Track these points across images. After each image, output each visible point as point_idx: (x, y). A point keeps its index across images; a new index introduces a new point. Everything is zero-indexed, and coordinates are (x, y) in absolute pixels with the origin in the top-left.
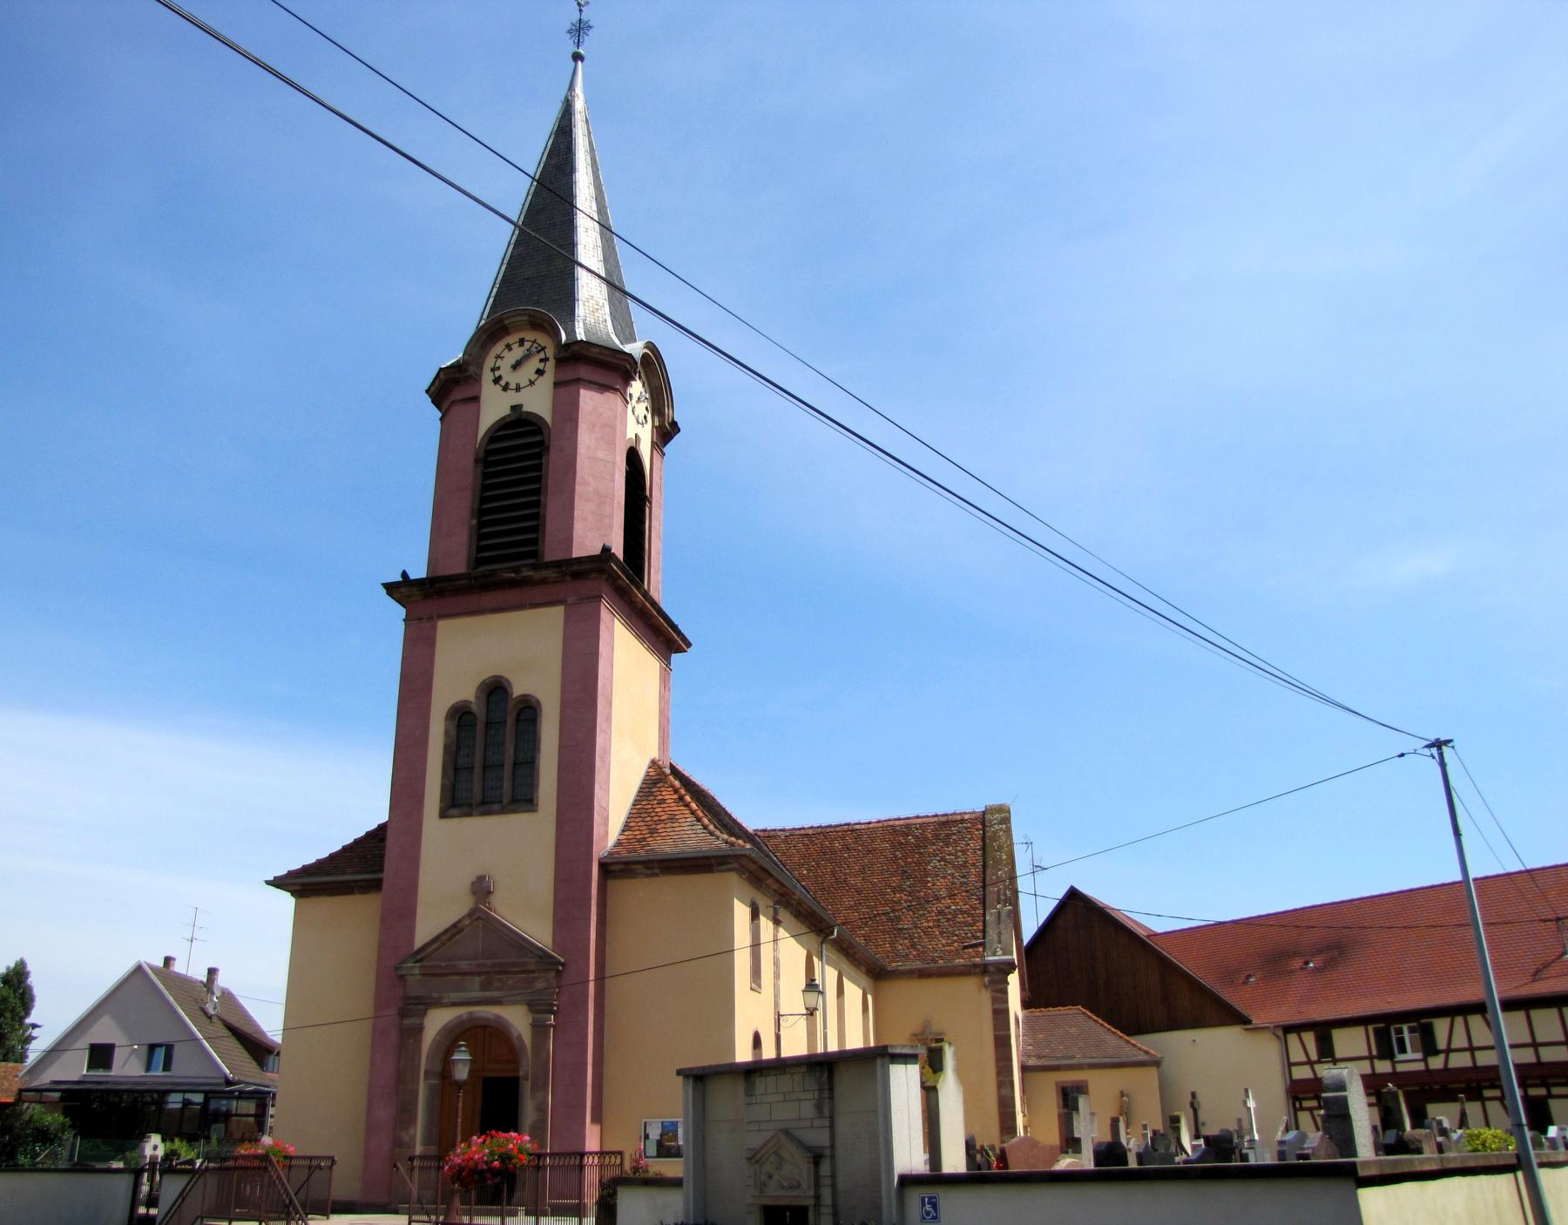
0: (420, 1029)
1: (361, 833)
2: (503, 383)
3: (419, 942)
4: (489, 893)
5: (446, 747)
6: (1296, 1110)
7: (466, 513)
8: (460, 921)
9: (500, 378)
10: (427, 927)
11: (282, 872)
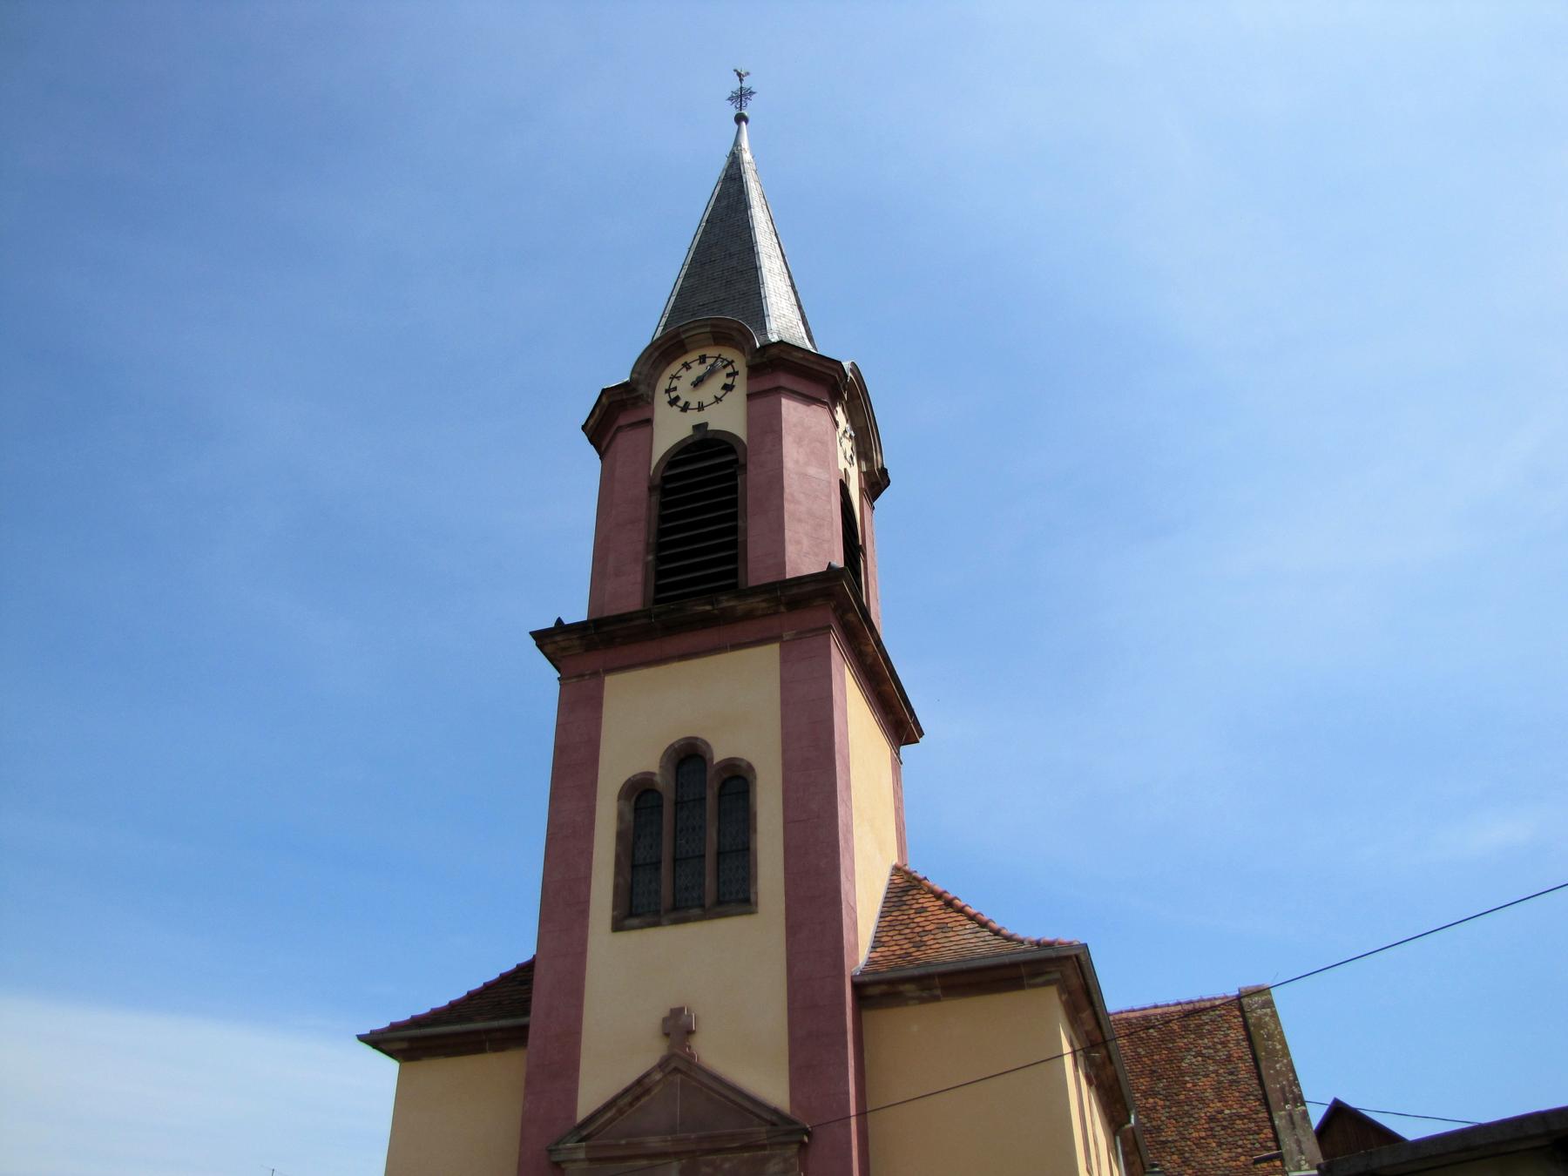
1: (493, 975)
2: (681, 403)
3: (582, 1112)
5: (620, 836)
7: (641, 547)
9: (677, 398)
10: (595, 1089)
11: (382, 1023)
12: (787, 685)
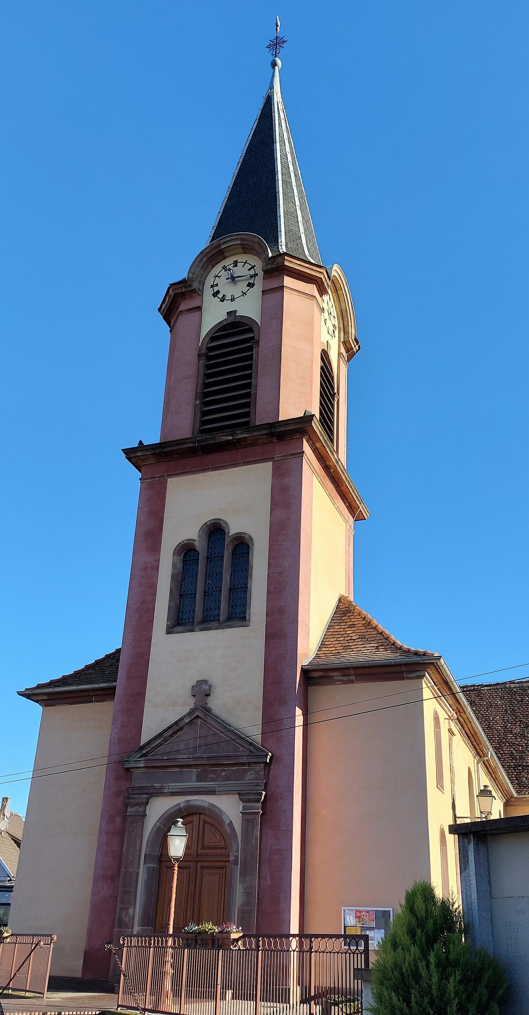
2: (220, 296)
5: (173, 577)
8: (181, 719)
9: (218, 292)
10: (153, 722)
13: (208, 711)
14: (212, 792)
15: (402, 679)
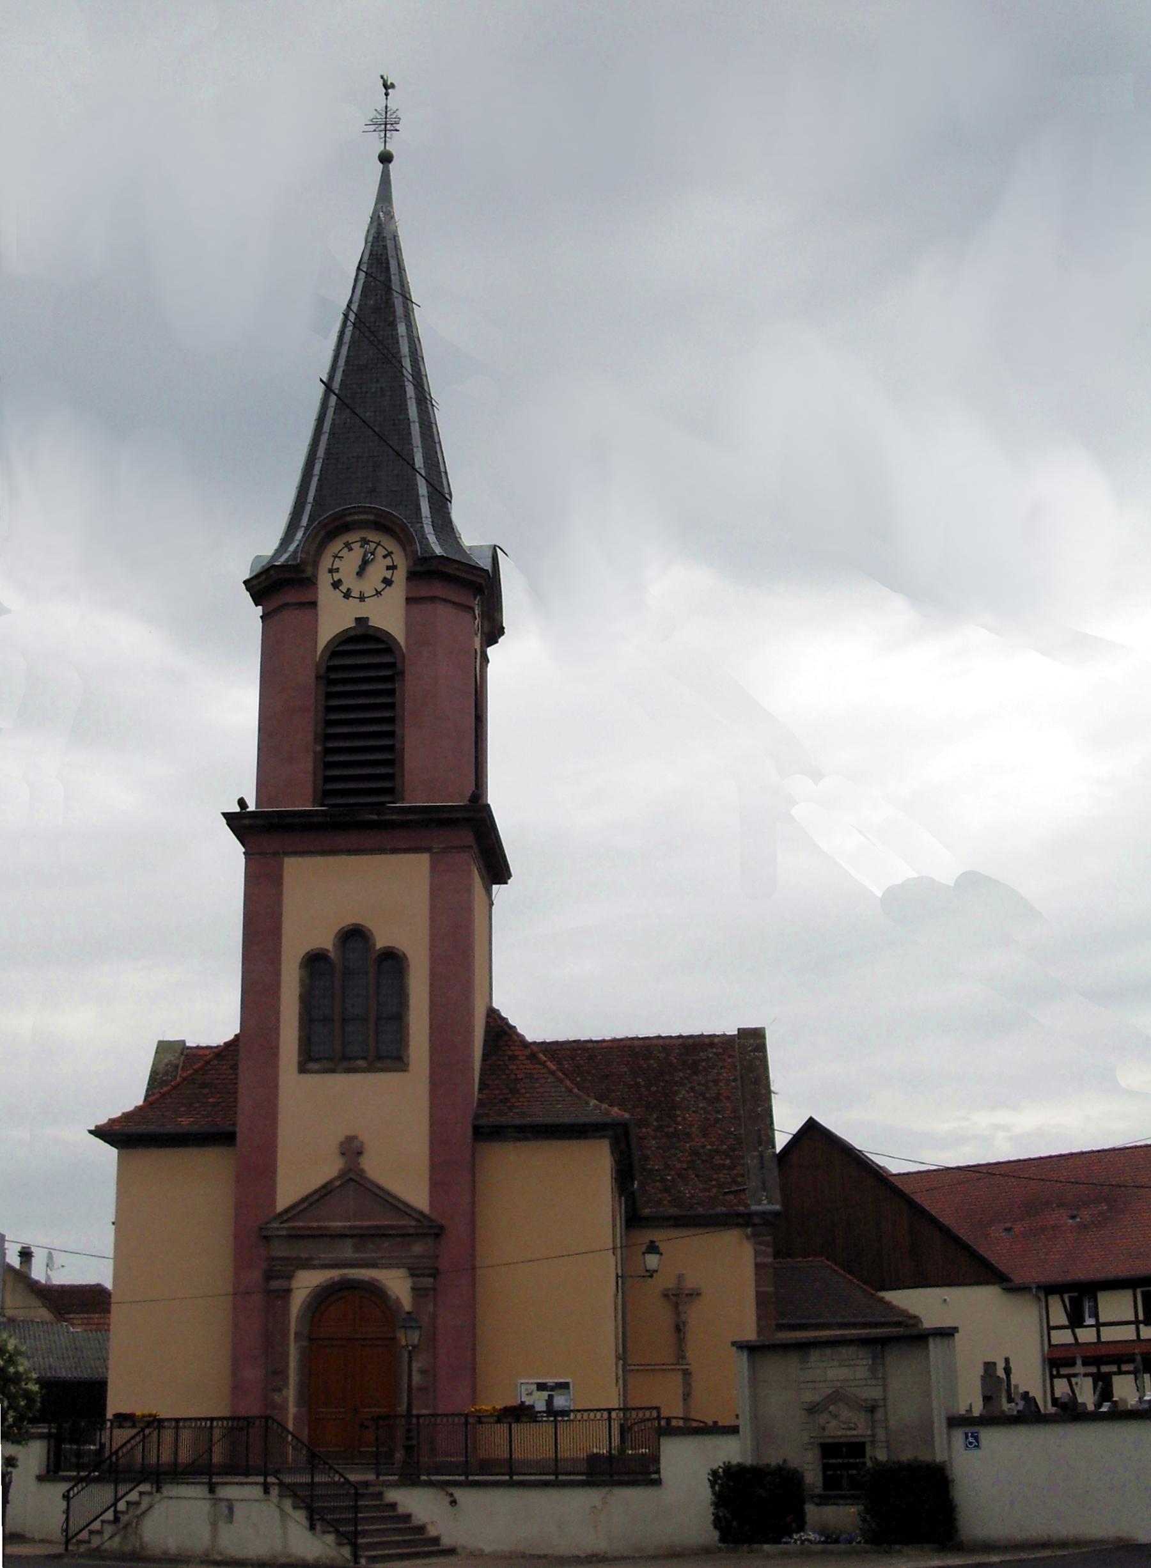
0: (288, 1291)
2: (344, 588)
4: (360, 1154)
6: (1052, 1377)
7: (310, 737)
10: (289, 1190)
11: (102, 1120)
12: (435, 892)
13: (361, 1172)
14: (373, 1265)
15: (586, 1138)
